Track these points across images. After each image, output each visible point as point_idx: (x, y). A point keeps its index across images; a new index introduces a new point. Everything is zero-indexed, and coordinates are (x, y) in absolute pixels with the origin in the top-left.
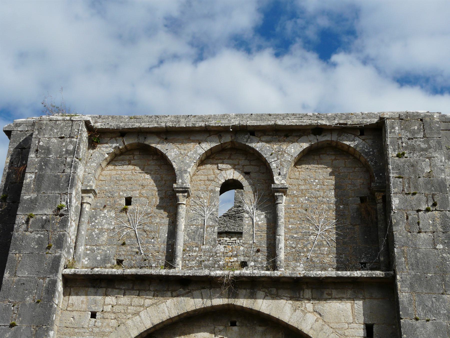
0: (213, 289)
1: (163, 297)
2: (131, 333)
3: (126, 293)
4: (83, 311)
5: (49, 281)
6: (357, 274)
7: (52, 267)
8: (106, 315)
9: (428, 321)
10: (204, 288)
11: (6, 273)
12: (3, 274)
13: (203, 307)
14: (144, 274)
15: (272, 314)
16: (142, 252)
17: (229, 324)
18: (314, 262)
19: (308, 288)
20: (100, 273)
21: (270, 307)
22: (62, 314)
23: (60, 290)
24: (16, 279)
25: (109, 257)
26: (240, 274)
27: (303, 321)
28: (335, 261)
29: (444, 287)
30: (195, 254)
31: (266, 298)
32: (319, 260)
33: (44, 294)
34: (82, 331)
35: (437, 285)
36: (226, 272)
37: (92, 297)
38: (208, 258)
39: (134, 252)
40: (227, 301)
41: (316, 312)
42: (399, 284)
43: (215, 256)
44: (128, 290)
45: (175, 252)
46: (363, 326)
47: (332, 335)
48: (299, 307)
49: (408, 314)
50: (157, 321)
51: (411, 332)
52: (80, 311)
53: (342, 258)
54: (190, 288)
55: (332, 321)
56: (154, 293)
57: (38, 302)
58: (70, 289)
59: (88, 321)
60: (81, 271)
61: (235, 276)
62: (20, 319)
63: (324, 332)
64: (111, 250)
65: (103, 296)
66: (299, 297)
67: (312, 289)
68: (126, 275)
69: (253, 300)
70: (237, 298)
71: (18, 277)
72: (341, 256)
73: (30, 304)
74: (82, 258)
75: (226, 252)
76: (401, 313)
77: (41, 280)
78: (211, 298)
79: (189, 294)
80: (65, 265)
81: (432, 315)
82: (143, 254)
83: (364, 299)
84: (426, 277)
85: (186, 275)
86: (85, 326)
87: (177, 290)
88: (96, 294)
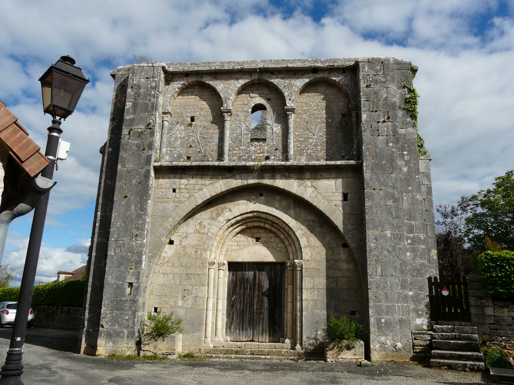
2: (198, 201)
6: (339, 163)
8: (182, 191)
9: (381, 190)
10: (242, 173)
13: (242, 185)
19: (308, 172)
23: (152, 176)
24: (125, 169)
26: (265, 164)
28: (325, 155)
30: (236, 152)
32: (315, 155)
34: (168, 200)
36: (256, 163)
37: (173, 180)
41: (313, 186)
44: (195, 175)
45: (224, 150)
46: (341, 194)
47: (323, 200)
49: (369, 187)
53: (330, 153)
57: (140, 183)
59: (171, 194)
60: (165, 164)
62: (130, 193)
66: (303, 178)
67: (311, 173)
68: (193, 166)
76: (365, 186)
77: (140, 170)
79: (233, 177)
83: (343, 178)
85: (231, 165)
86: (170, 197)
88: (175, 178)
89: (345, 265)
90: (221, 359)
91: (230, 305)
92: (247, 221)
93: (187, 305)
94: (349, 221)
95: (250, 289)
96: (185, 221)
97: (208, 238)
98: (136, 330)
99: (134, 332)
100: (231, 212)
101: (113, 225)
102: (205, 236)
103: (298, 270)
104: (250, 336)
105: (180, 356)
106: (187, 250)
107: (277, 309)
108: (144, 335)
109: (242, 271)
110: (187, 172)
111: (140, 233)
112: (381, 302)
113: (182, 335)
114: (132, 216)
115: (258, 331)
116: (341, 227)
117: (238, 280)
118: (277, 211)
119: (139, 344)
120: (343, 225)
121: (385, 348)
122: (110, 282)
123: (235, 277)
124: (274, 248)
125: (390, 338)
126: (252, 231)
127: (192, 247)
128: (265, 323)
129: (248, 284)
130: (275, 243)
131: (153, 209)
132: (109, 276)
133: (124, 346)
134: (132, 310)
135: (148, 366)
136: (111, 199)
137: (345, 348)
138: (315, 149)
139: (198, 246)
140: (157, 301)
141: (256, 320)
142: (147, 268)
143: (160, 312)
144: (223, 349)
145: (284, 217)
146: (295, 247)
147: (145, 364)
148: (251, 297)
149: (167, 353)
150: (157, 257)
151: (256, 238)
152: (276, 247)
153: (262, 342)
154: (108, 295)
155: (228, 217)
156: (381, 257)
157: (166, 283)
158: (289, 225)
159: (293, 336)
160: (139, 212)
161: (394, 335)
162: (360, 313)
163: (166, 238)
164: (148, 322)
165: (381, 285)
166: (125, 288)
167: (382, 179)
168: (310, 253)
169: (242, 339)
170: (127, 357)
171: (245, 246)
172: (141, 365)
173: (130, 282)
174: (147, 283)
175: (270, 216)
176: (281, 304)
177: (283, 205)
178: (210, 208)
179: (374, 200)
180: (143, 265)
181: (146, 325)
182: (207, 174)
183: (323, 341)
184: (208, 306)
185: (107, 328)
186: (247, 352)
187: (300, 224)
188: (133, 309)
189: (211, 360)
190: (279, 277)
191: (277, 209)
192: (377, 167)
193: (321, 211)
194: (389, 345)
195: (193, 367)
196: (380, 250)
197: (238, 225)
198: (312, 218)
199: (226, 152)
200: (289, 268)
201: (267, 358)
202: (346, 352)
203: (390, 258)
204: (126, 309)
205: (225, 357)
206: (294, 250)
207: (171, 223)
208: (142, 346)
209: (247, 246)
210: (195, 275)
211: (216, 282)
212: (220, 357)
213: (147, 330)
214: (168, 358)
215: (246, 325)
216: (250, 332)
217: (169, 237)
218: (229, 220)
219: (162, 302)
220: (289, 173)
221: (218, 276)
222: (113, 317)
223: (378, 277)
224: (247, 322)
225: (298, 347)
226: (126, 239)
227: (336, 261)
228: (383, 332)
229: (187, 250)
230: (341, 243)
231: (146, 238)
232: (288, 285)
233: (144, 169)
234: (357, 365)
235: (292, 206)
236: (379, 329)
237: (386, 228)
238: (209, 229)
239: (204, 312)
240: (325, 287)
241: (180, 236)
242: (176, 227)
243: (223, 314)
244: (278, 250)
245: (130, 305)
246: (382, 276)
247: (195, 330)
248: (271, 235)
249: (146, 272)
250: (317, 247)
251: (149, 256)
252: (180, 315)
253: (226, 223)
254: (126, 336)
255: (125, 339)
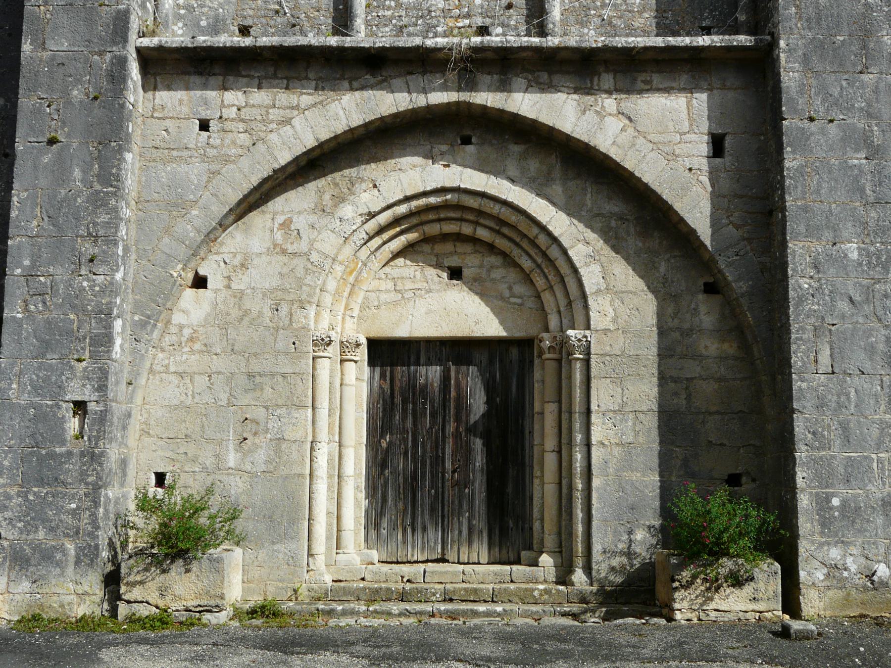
0: (428, 74)
1: (334, 90)
2: (278, 157)
3: (263, 85)
4: (185, 119)
5: (112, 59)
6: (703, 41)
7: (115, 32)
8: (228, 125)
9: (831, 121)
10: (411, 73)
11: (25, 43)
12: (20, 47)
13: (410, 107)
14: (295, 44)
15: (541, 120)
16: (287, 11)
17: (459, 142)
18: (614, 26)
19: (607, 71)
20: (209, 44)
21: (537, 106)
22: (144, 124)
23: (135, 78)
24: (46, 55)
25: (223, 20)
26: (482, 42)
27: (599, 131)
28: (654, 25)
29: (864, 60)
30: (388, 13)
31: (529, 89)
32: (624, 22)
33: (105, 83)
34: (185, 153)
35: (853, 57)
36: (456, 40)
37: (198, 93)
38: (414, 20)
39: (271, 10)
40: (457, 96)
41: (623, 114)
42: (782, 56)
43: (428, 17)
44: (266, 78)
45: (351, 7)
46: (706, 137)
47: (652, 154)
48: (592, 106)
49: (796, 111)
50: (325, 135)
51: (800, 141)
52: (178, 118)
53: (667, 18)
54: (384, 73)
55: (651, 131)
56: (317, 83)
57: (96, 98)
58: (155, 78)
59: (194, 136)
60: (173, 42)
61: (473, 47)
62: (66, 129)
63: (637, 150)
64: (226, 7)
65: (220, 90)
66: (592, 88)
67: (615, 72)
68: (260, 47)
69: (506, 93)
70: (475, 92)
71: (51, 51)
72: (665, 15)
73: (81, 102)
74: (170, 22)
75: (449, 10)
76: (784, 109)
77: (96, 57)
78: (425, 91)
79: (383, 84)
80: (139, 32)
81: (838, 112)
82: (288, 15)
83: (710, 89)
84: (834, 43)
85: (377, 45)
86: (191, 146)
87: (360, 78)
88: (205, 87)
89: (712, 343)
90: (363, 621)
91: (375, 462)
92: (424, 218)
93: (253, 463)
94: (728, 217)
95: (433, 415)
96: (239, 218)
97: (310, 266)
98: (103, 542)
99: (97, 547)
100: (376, 190)
101: (18, 227)
102: (300, 263)
103: (578, 359)
104: (434, 549)
105: (238, 614)
106: (247, 304)
107: (511, 471)
108: (126, 557)
109: (409, 366)
110: (241, 68)
111: (104, 252)
112: (829, 449)
113: (241, 550)
114: (76, 200)
115: (457, 532)
116: (704, 232)
117: (397, 389)
118: (513, 187)
119: (112, 581)
120: (712, 226)
121: (842, 580)
122: (14, 401)
123: (388, 381)
124: (502, 298)
125: (855, 552)
126: (439, 248)
127: (264, 295)
128: (477, 509)
129: (426, 400)
130: (506, 282)
131: (139, 182)
132: (9, 385)
133: (68, 589)
134: (87, 484)
135: (142, 656)
136: (7, 151)
137: (726, 582)
138: (624, 7)
139: (279, 293)
140: (162, 454)
141: (453, 502)
142: (130, 359)
143: (171, 487)
144: (364, 589)
145: (534, 204)
146: (567, 294)
147: (133, 648)
148: (437, 438)
149: (200, 606)
150: (159, 325)
151: (449, 268)
152: (507, 293)
153: (468, 563)
154: (11, 439)
155: (370, 205)
156: (829, 320)
157: (189, 401)
158: (550, 228)
159: (560, 546)
160: (98, 187)
161: (868, 542)
162: (754, 480)
163: (183, 269)
164: (138, 519)
165: (830, 401)
166: (64, 417)
167: (835, 87)
168: (611, 310)
169: (413, 555)
170: (77, 622)
171: (417, 293)
172: (121, 650)
173: (79, 398)
174: (131, 403)
175: (491, 204)
176: (523, 457)
177: (532, 169)
178: (315, 179)
179: (811, 151)
180: (117, 348)
181: (132, 528)
182: (303, 75)
183: (650, 558)
184: (315, 466)
185: (12, 538)
186: (434, 594)
187: (581, 226)
188: (90, 479)
189: (332, 622)
190: (515, 380)
191: (512, 181)
192: (819, 52)
193: (646, 185)
194: (853, 570)
195: (286, 653)
196: (827, 298)
197: (398, 229)
198: (616, 209)
199: (358, 12)
200: (547, 356)
201: (495, 611)
202: (728, 591)
203: (857, 322)
204: (70, 480)
205: (372, 612)
206: (563, 302)
207: (198, 223)
208: (123, 589)
209: (423, 292)
210: (273, 375)
211: (335, 397)
212: (358, 613)
213: (136, 541)
214: (204, 621)
215: (423, 516)
216: (434, 535)
217: (192, 265)
218: (372, 215)
219: (179, 457)
220: (550, 73)
221: (342, 379)
222: (30, 506)
223: (823, 377)
224: (427, 507)
225: (579, 577)
226: (60, 270)
227: (687, 333)
228: (836, 535)
229: (247, 304)
230: (701, 283)
231: (122, 268)
232: (544, 402)
233: (108, 56)
234: (775, 634)
235: (557, 173)
236: (823, 525)
237: (845, 234)
238: (312, 243)
239: (303, 484)
240: (655, 407)
241: (225, 263)
242: (212, 236)
243: (358, 487)
244: (514, 304)
245: (80, 467)
246: (833, 373)
247: (280, 535)
248: (494, 260)
249: (127, 369)
250: (631, 292)
251: (135, 324)
252: (233, 492)
253: (364, 223)
254: (72, 559)
255: (70, 570)
